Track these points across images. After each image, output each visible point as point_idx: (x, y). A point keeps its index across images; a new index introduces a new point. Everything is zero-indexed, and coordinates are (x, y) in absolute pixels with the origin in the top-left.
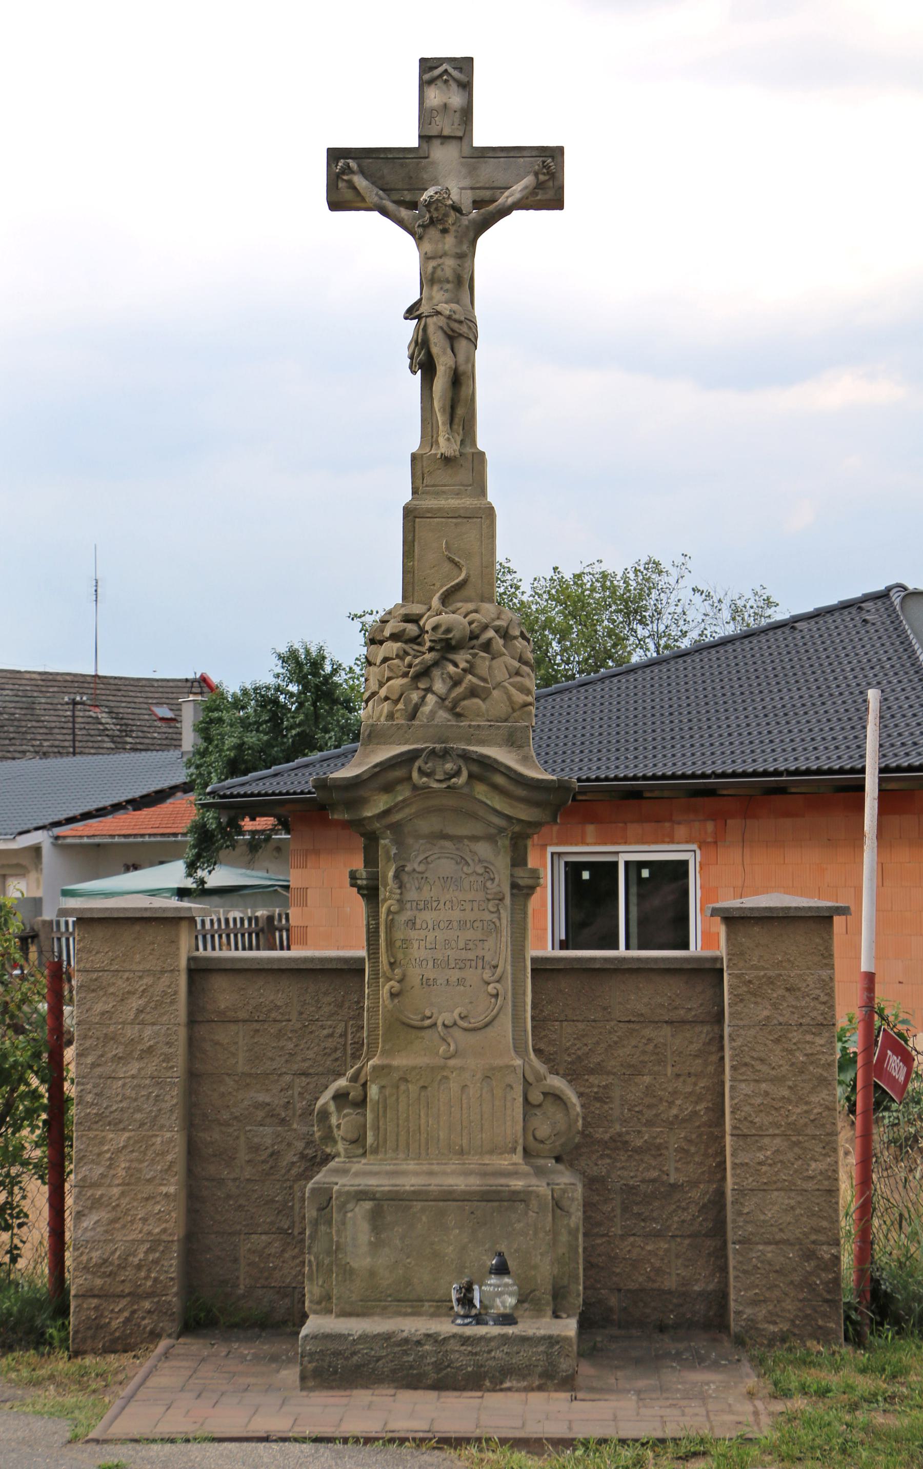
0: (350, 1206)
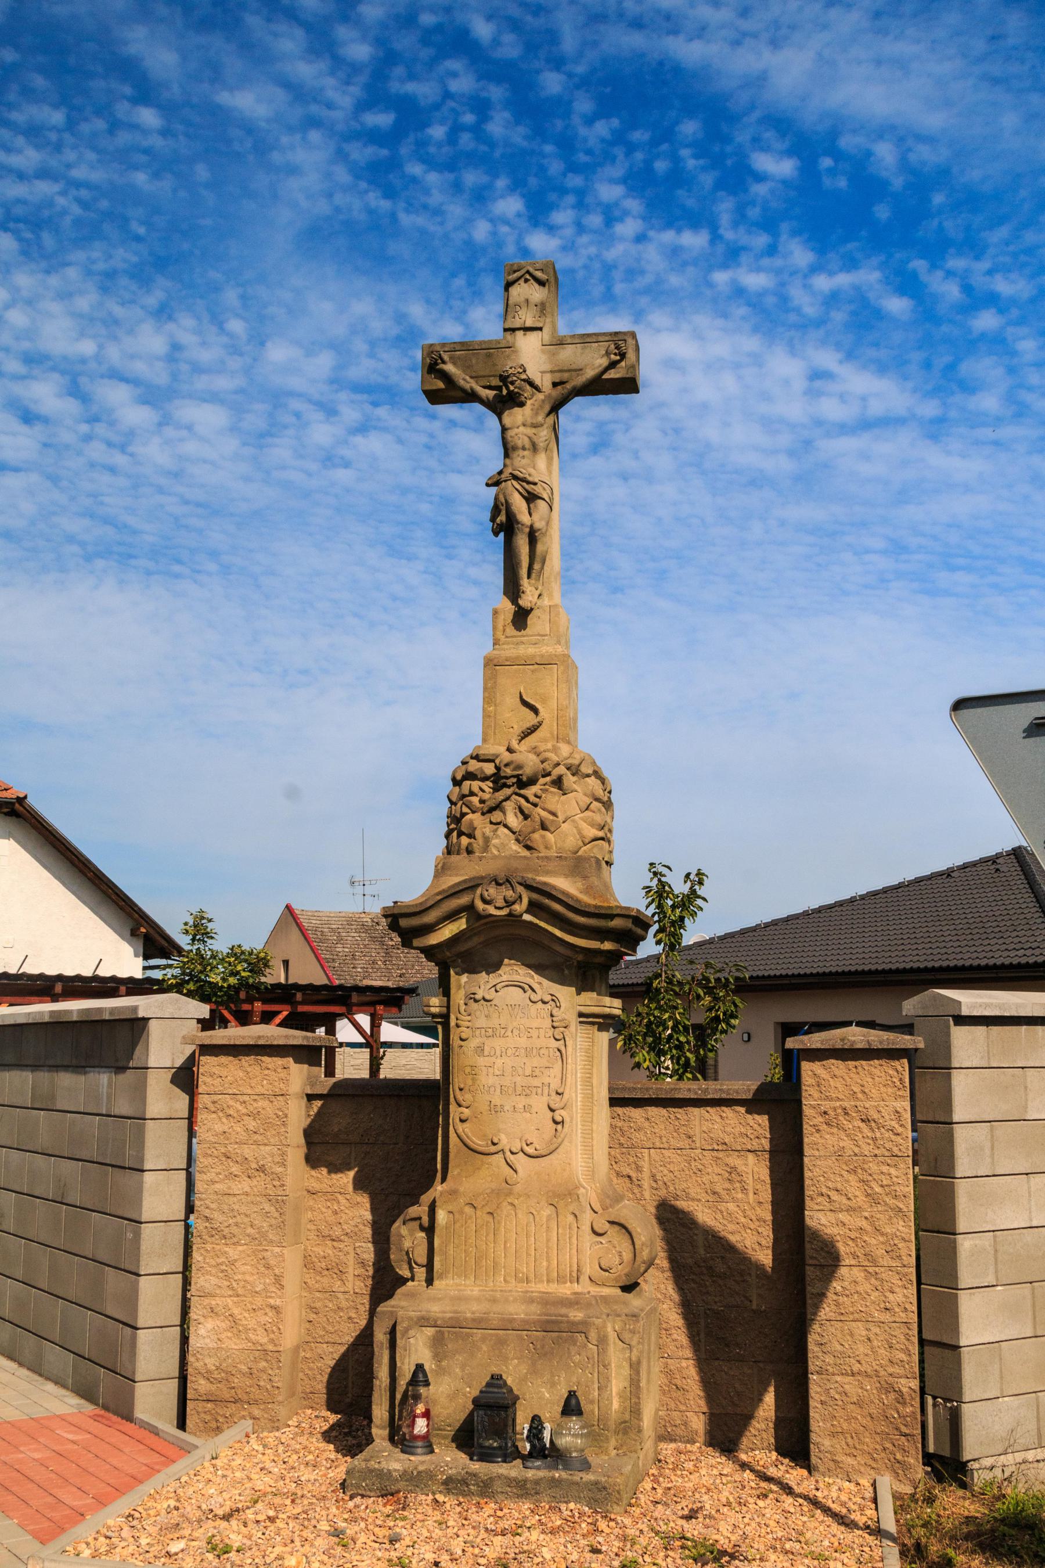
0: (411, 1333)
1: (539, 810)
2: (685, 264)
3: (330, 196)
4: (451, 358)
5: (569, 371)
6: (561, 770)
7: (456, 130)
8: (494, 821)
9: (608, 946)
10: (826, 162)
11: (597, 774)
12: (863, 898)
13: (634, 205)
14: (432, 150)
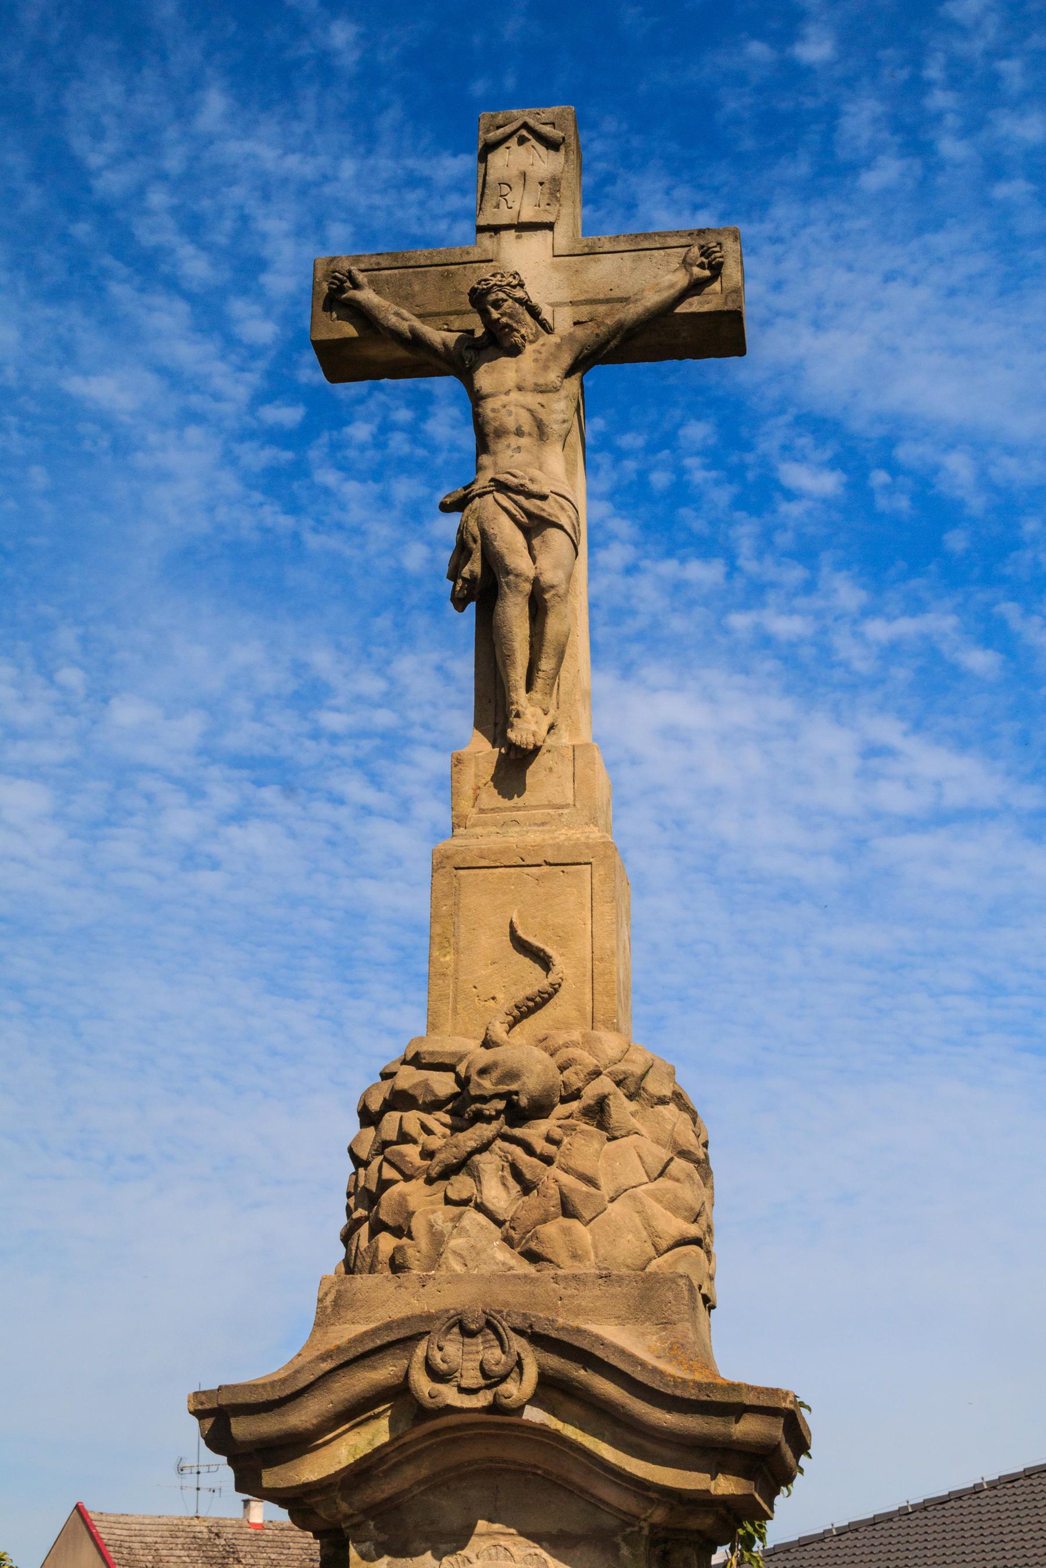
1: (554, 1171)
2: (691, 604)
3: (210, 509)
4: (371, 282)
5: (607, 301)
6: (604, 1085)
7: (386, 428)
8: (453, 1195)
9: (725, 1486)
10: (880, 477)
11: (678, 1098)
12: (993, 1486)
13: (622, 526)
14: (352, 453)
